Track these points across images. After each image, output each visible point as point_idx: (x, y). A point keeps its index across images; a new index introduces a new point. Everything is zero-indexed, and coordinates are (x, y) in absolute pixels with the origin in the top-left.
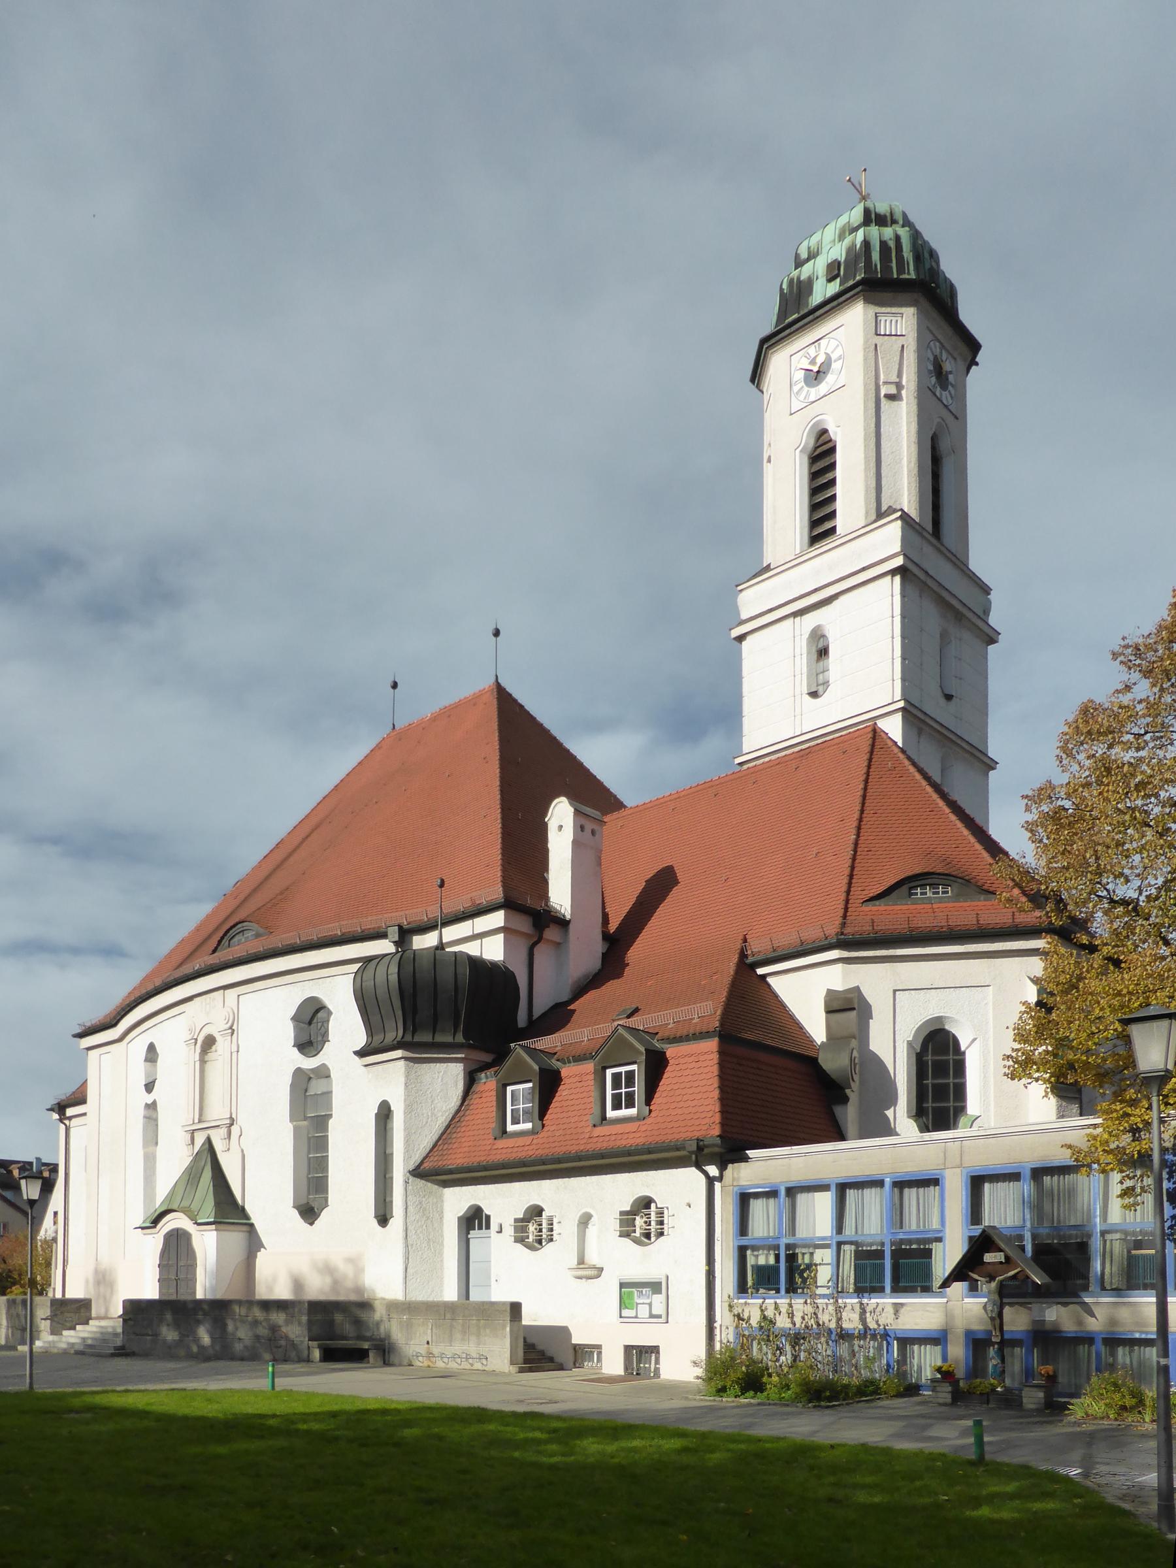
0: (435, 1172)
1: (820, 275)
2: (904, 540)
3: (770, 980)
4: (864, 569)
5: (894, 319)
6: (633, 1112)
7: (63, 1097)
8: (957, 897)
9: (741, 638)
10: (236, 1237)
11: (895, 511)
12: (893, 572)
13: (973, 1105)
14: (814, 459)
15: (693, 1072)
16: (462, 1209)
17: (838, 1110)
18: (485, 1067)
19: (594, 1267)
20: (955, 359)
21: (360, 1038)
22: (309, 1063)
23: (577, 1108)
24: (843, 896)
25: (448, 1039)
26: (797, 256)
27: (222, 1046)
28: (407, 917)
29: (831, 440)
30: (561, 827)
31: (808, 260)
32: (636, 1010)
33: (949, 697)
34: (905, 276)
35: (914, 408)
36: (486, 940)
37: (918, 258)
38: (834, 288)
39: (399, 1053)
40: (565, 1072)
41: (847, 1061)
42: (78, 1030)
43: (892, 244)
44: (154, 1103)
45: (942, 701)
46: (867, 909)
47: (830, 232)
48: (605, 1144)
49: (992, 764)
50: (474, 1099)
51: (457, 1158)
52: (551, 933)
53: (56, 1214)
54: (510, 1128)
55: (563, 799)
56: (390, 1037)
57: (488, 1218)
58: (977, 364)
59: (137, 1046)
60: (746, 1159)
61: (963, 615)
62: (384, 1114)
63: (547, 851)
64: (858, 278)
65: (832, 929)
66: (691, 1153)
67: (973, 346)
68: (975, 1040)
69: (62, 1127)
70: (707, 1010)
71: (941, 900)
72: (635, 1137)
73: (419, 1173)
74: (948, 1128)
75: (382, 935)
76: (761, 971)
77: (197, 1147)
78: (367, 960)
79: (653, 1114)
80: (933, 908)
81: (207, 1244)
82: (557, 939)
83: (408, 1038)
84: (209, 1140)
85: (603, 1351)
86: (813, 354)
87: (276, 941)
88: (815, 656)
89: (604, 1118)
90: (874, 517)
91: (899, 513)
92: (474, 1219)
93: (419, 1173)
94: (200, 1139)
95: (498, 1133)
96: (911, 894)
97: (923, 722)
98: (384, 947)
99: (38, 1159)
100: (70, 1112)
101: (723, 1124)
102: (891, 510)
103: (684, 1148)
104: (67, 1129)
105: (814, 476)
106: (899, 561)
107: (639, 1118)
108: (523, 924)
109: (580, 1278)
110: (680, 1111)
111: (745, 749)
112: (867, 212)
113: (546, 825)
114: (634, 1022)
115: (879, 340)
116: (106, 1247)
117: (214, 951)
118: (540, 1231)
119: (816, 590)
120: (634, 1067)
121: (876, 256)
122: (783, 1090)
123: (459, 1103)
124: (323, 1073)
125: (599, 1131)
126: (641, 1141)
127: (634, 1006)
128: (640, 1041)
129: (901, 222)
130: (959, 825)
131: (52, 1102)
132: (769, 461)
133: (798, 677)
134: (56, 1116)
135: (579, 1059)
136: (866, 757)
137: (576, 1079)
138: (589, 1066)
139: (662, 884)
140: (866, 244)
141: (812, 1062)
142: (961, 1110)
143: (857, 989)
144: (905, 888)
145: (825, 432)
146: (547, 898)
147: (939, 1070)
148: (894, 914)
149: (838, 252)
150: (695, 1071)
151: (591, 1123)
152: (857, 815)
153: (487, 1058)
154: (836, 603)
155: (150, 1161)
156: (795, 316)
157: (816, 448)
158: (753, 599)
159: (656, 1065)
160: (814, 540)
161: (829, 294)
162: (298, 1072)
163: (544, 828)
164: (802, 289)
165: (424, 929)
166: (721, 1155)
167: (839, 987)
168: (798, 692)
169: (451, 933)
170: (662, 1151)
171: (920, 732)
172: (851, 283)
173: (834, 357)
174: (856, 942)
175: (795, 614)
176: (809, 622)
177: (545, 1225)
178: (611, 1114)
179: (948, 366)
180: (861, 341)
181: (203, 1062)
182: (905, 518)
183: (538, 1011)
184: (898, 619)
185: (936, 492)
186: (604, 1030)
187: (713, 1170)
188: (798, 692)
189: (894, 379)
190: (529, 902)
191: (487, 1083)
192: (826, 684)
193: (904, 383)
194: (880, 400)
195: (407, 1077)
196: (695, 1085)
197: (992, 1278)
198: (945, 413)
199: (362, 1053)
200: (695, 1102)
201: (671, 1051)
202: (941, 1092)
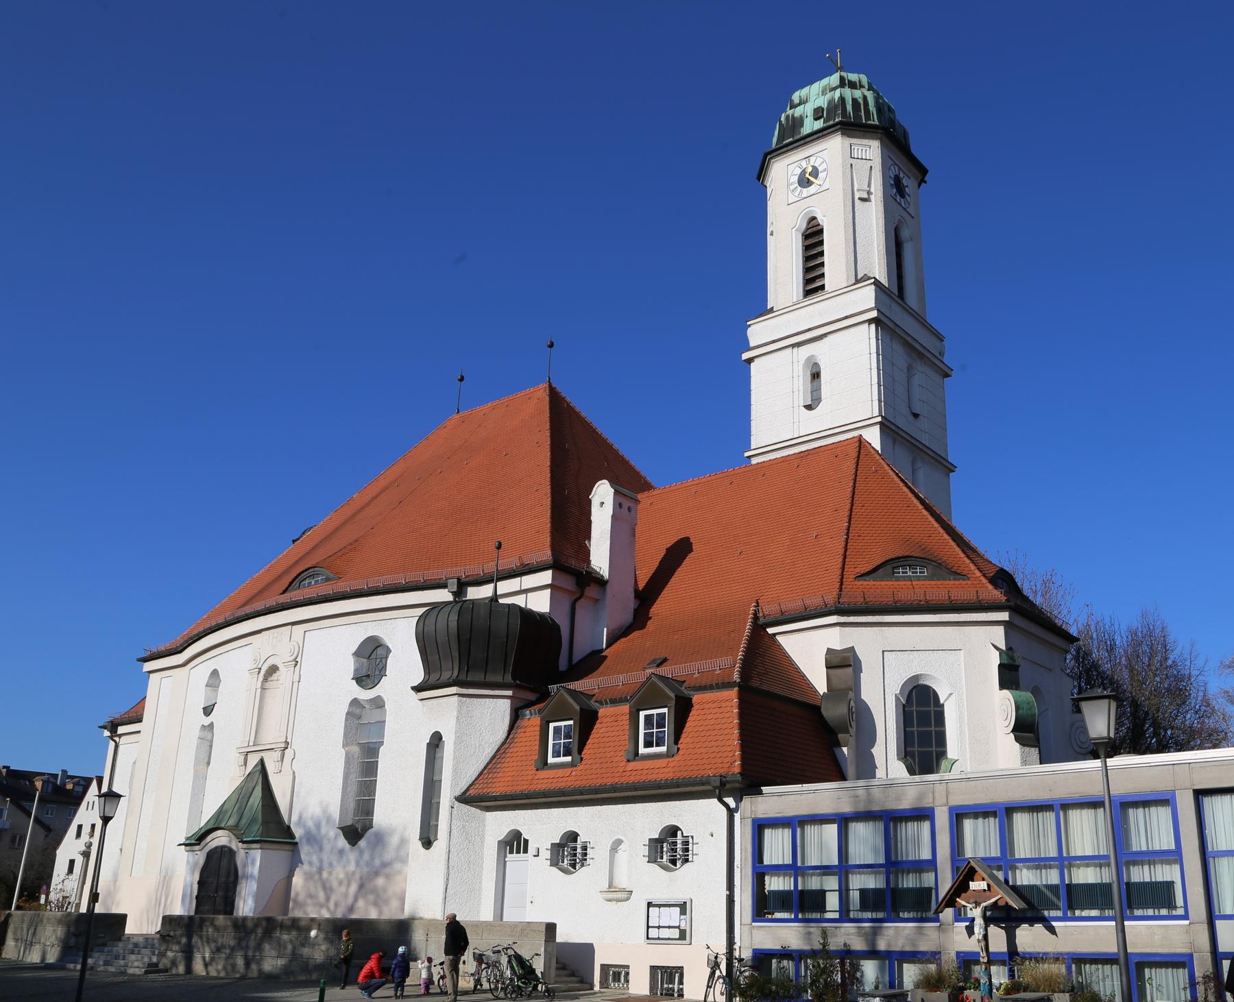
0: (477, 798)
2: (877, 299)
3: (779, 638)
4: (846, 318)
6: (663, 749)
7: (117, 716)
8: (931, 578)
9: (750, 361)
10: (280, 856)
11: (870, 278)
12: (870, 321)
13: (952, 751)
14: (806, 236)
16: (502, 834)
18: (529, 704)
19: (624, 890)
21: (418, 674)
22: (365, 695)
24: (839, 572)
25: (499, 679)
26: (792, 101)
27: (284, 675)
28: (463, 572)
30: (602, 503)
31: (800, 104)
32: (665, 660)
33: (916, 416)
35: (881, 208)
36: (535, 594)
37: (879, 111)
38: (819, 124)
39: (454, 690)
40: (601, 712)
42: (143, 655)
43: (861, 101)
44: (211, 726)
45: (911, 418)
47: (816, 87)
48: (638, 778)
50: (519, 734)
51: (499, 787)
52: (592, 591)
53: (80, 827)
54: (551, 760)
55: (605, 481)
56: (446, 676)
57: (526, 841)
59: (201, 671)
60: (760, 793)
62: (436, 741)
63: (590, 522)
65: (831, 598)
66: (715, 788)
67: (923, 171)
69: (112, 744)
70: (731, 664)
71: (918, 578)
72: (665, 772)
73: (464, 799)
74: (931, 772)
75: (443, 586)
77: (249, 769)
78: (434, 607)
81: (253, 862)
83: (463, 677)
84: (262, 762)
85: (631, 971)
87: (342, 586)
89: (637, 754)
92: (515, 843)
93: (464, 799)
94: (253, 761)
95: (631, 756)
98: (444, 595)
99: (64, 772)
100: (121, 730)
101: (744, 758)
102: (866, 278)
103: (708, 783)
104: (117, 746)
105: (807, 248)
106: (874, 314)
107: (668, 755)
108: (568, 583)
109: (610, 900)
110: (704, 751)
112: (842, 79)
113: (590, 501)
114: (662, 671)
115: (854, 162)
116: (135, 862)
117: (284, 592)
118: (575, 855)
120: (665, 710)
121: (849, 108)
122: (792, 735)
123: (504, 736)
124: (378, 703)
125: (632, 765)
126: (670, 776)
127: (663, 656)
128: (672, 688)
130: (931, 519)
131: (105, 720)
132: (772, 234)
134: (107, 733)
135: (614, 702)
137: (611, 718)
138: (625, 708)
139: (679, 551)
140: (842, 99)
141: (817, 709)
142: (942, 754)
144: (889, 567)
145: (814, 218)
146: (589, 562)
147: (922, 714)
148: (880, 588)
149: (823, 102)
152: (848, 506)
153: (532, 697)
154: (825, 340)
155: (200, 780)
157: (807, 229)
158: (758, 332)
159: (683, 709)
160: (808, 293)
161: (816, 128)
162: (355, 702)
163: (589, 503)
164: (798, 122)
165: (479, 583)
166: (741, 789)
169: (504, 587)
170: (686, 785)
171: (894, 441)
172: (831, 123)
173: (820, 169)
174: (848, 608)
175: (793, 346)
177: (579, 850)
178: (642, 750)
179: (905, 182)
181: (263, 688)
182: (877, 283)
183: (577, 657)
184: (874, 356)
185: (900, 266)
186: (640, 676)
187: (731, 802)
190: (573, 563)
191: (532, 720)
193: (872, 190)
194: (858, 200)
195: (459, 711)
196: (718, 723)
197: (977, 904)
198: (904, 214)
199: (418, 689)
202: (925, 739)
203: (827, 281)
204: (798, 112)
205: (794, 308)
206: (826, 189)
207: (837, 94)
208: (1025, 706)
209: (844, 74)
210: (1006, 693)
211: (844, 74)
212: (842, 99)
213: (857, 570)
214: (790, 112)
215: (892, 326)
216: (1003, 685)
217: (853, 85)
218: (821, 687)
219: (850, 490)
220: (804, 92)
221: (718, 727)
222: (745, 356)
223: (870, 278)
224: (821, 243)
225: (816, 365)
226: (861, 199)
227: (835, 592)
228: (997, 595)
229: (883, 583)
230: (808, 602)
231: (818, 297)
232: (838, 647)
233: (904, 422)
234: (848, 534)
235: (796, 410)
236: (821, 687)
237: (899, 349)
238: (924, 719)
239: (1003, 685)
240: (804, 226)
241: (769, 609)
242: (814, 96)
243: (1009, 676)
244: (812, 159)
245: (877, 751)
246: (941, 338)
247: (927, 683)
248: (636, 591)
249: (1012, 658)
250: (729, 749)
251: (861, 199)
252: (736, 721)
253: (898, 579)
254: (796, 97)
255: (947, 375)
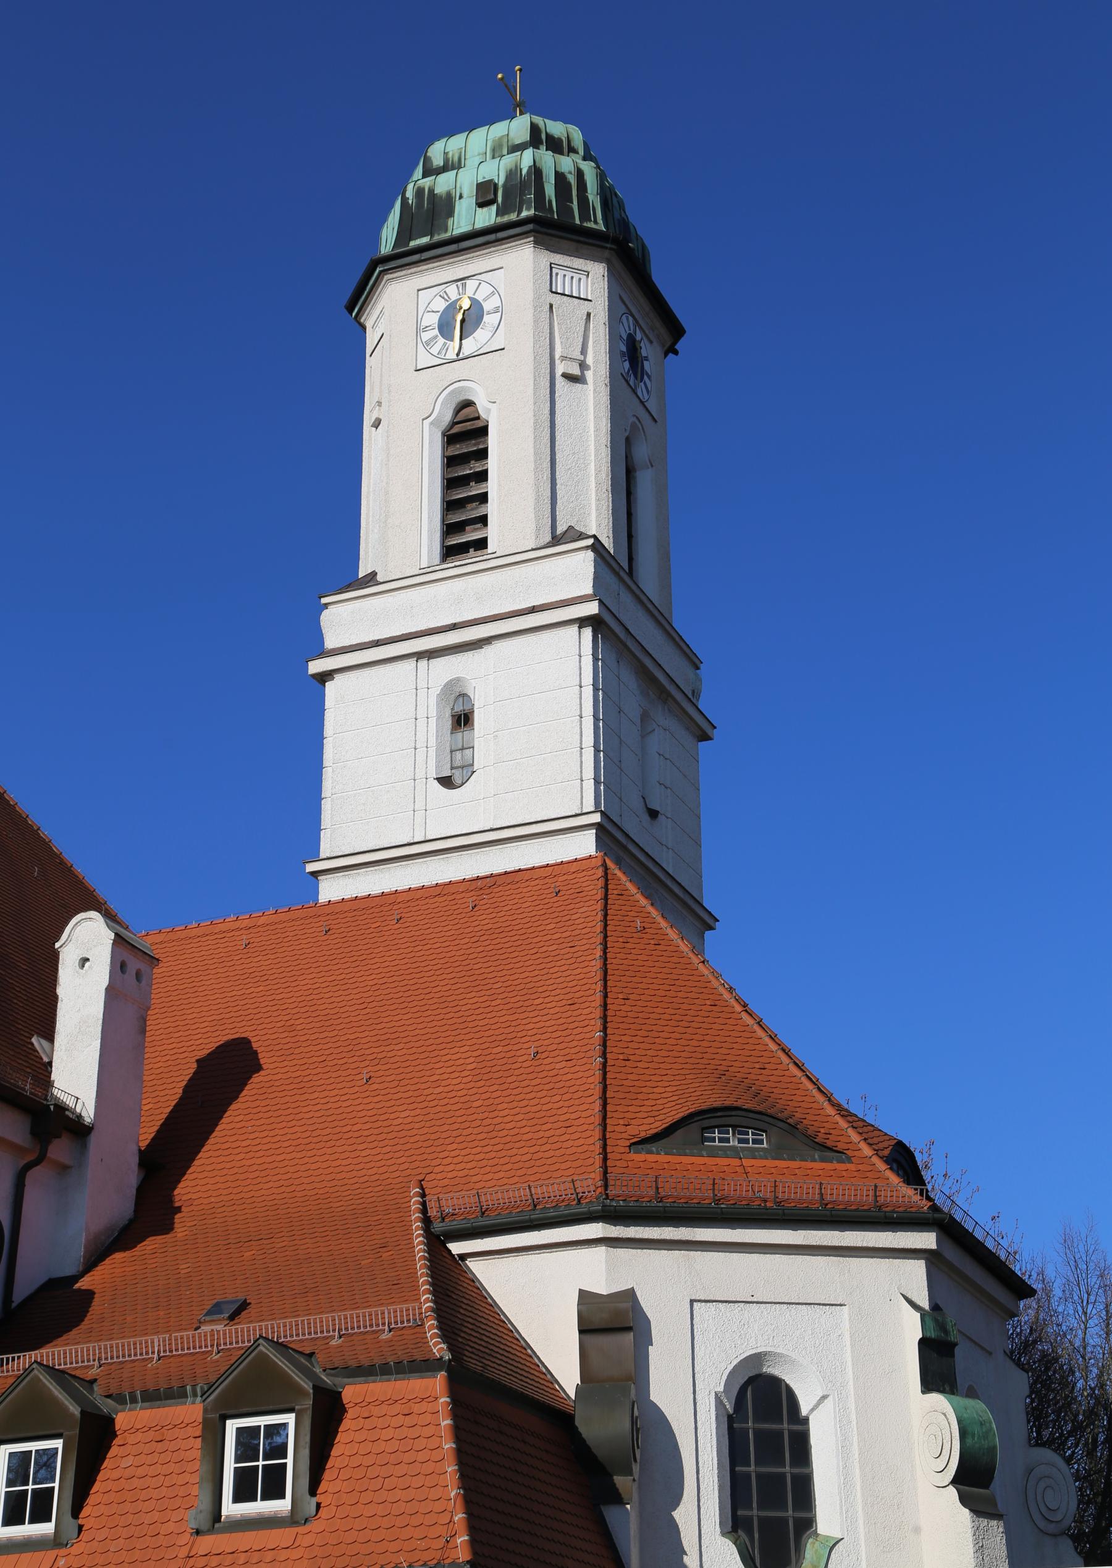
1: (465, 195)
4: (533, 610)
5: (576, 277)
8: (776, 1152)
9: (324, 677)
11: (581, 536)
12: (582, 622)
14: (451, 438)
15: (399, 1433)
17: (611, 1513)
20: (651, 342)
23: (156, 1494)
26: (427, 160)
29: (478, 418)
31: (445, 168)
32: (244, 1306)
33: (653, 814)
34: (591, 225)
38: (487, 217)
40: (122, 1420)
41: (627, 1424)
43: (572, 179)
45: (646, 817)
46: (633, 1156)
47: (479, 140)
49: (710, 921)
52: (60, 1149)
58: (676, 353)
61: (669, 695)
64: (525, 214)
67: (676, 331)
68: (824, 1397)
71: (753, 1154)
76: (457, 1248)
79: (323, 1513)
80: (742, 1164)
82: (65, 1160)
86: (454, 296)
88: (448, 723)
90: (548, 538)
91: (591, 541)
96: (704, 1140)
97: (624, 848)
101: (473, 1527)
102: (573, 535)
106: (592, 608)
111: (325, 850)
112: (535, 129)
115: (556, 300)
119: (454, 627)
121: (550, 190)
125: (207, 1543)
129: (581, 152)
132: (377, 424)
133: (421, 752)
135: (152, 1397)
136: (600, 906)
138: (192, 1411)
139: (227, 1071)
140: (537, 171)
143: (630, 1294)
144: (695, 1128)
145: (468, 404)
146: (48, 1084)
148: (685, 1171)
149: (496, 171)
150: (404, 1432)
151: (193, 1525)
156: (425, 240)
157: (454, 424)
158: (343, 620)
160: (450, 552)
163: (52, 960)
164: (439, 208)
167: (602, 1287)
168: (420, 774)
172: (513, 217)
173: (487, 306)
174: (629, 1212)
175: (419, 655)
176: (444, 669)
178: (230, 1509)
179: (646, 349)
180: (530, 296)
184: (588, 691)
188: (420, 774)
189: (577, 354)
192: (469, 769)
193: (590, 360)
200: (411, 1493)
201: (350, 1393)
203: (493, 532)
204: (443, 184)
205: (516, 560)
206: (485, 349)
207: (527, 159)
208: (976, 1429)
209: (539, 120)
210: (937, 1399)
211: (539, 120)
212: (537, 171)
213: (632, 1130)
214: (427, 182)
215: (622, 634)
216: (928, 1385)
217: (555, 145)
218: (568, 1375)
219: (598, 964)
220: (454, 144)
221: (408, 1458)
222: (316, 667)
223: (581, 536)
224: (482, 454)
225: (463, 695)
226: (568, 377)
227: (597, 1174)
228: (898, 1192)
229: (686, 1160)
230: (538, 1192)
231: (472, 561)
232: (603, 1289)
233: (634, 825)
234: (604, 1054)
235: (420, 784)
236: (568, 1375)
237: (630, 680)
238: (770, 1447)
239: (928, 1385)
240: (448, 417)
241: (453, 1202)
242: (476, 158)
243: (939, 1366)
244: (471, 284)
245: (684, 1515)
246: (695, 663)
247: (776, 1371)
248: (140, 1150)
249: (942, 1327)
250: (438, 1506)
251: (568, 377)
252: (449, 1445)
253: (713, 1153)
254: (437, 152)
255: (705, 737)
